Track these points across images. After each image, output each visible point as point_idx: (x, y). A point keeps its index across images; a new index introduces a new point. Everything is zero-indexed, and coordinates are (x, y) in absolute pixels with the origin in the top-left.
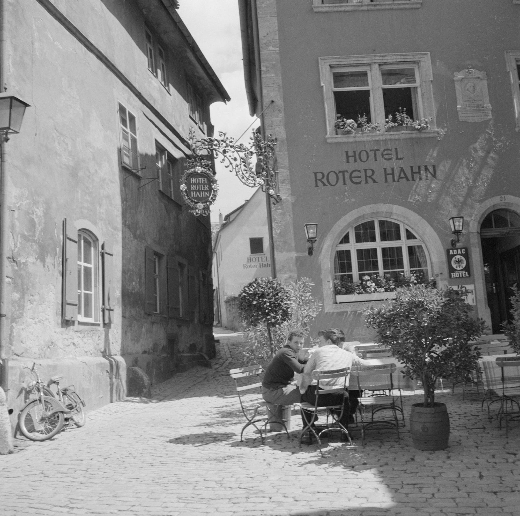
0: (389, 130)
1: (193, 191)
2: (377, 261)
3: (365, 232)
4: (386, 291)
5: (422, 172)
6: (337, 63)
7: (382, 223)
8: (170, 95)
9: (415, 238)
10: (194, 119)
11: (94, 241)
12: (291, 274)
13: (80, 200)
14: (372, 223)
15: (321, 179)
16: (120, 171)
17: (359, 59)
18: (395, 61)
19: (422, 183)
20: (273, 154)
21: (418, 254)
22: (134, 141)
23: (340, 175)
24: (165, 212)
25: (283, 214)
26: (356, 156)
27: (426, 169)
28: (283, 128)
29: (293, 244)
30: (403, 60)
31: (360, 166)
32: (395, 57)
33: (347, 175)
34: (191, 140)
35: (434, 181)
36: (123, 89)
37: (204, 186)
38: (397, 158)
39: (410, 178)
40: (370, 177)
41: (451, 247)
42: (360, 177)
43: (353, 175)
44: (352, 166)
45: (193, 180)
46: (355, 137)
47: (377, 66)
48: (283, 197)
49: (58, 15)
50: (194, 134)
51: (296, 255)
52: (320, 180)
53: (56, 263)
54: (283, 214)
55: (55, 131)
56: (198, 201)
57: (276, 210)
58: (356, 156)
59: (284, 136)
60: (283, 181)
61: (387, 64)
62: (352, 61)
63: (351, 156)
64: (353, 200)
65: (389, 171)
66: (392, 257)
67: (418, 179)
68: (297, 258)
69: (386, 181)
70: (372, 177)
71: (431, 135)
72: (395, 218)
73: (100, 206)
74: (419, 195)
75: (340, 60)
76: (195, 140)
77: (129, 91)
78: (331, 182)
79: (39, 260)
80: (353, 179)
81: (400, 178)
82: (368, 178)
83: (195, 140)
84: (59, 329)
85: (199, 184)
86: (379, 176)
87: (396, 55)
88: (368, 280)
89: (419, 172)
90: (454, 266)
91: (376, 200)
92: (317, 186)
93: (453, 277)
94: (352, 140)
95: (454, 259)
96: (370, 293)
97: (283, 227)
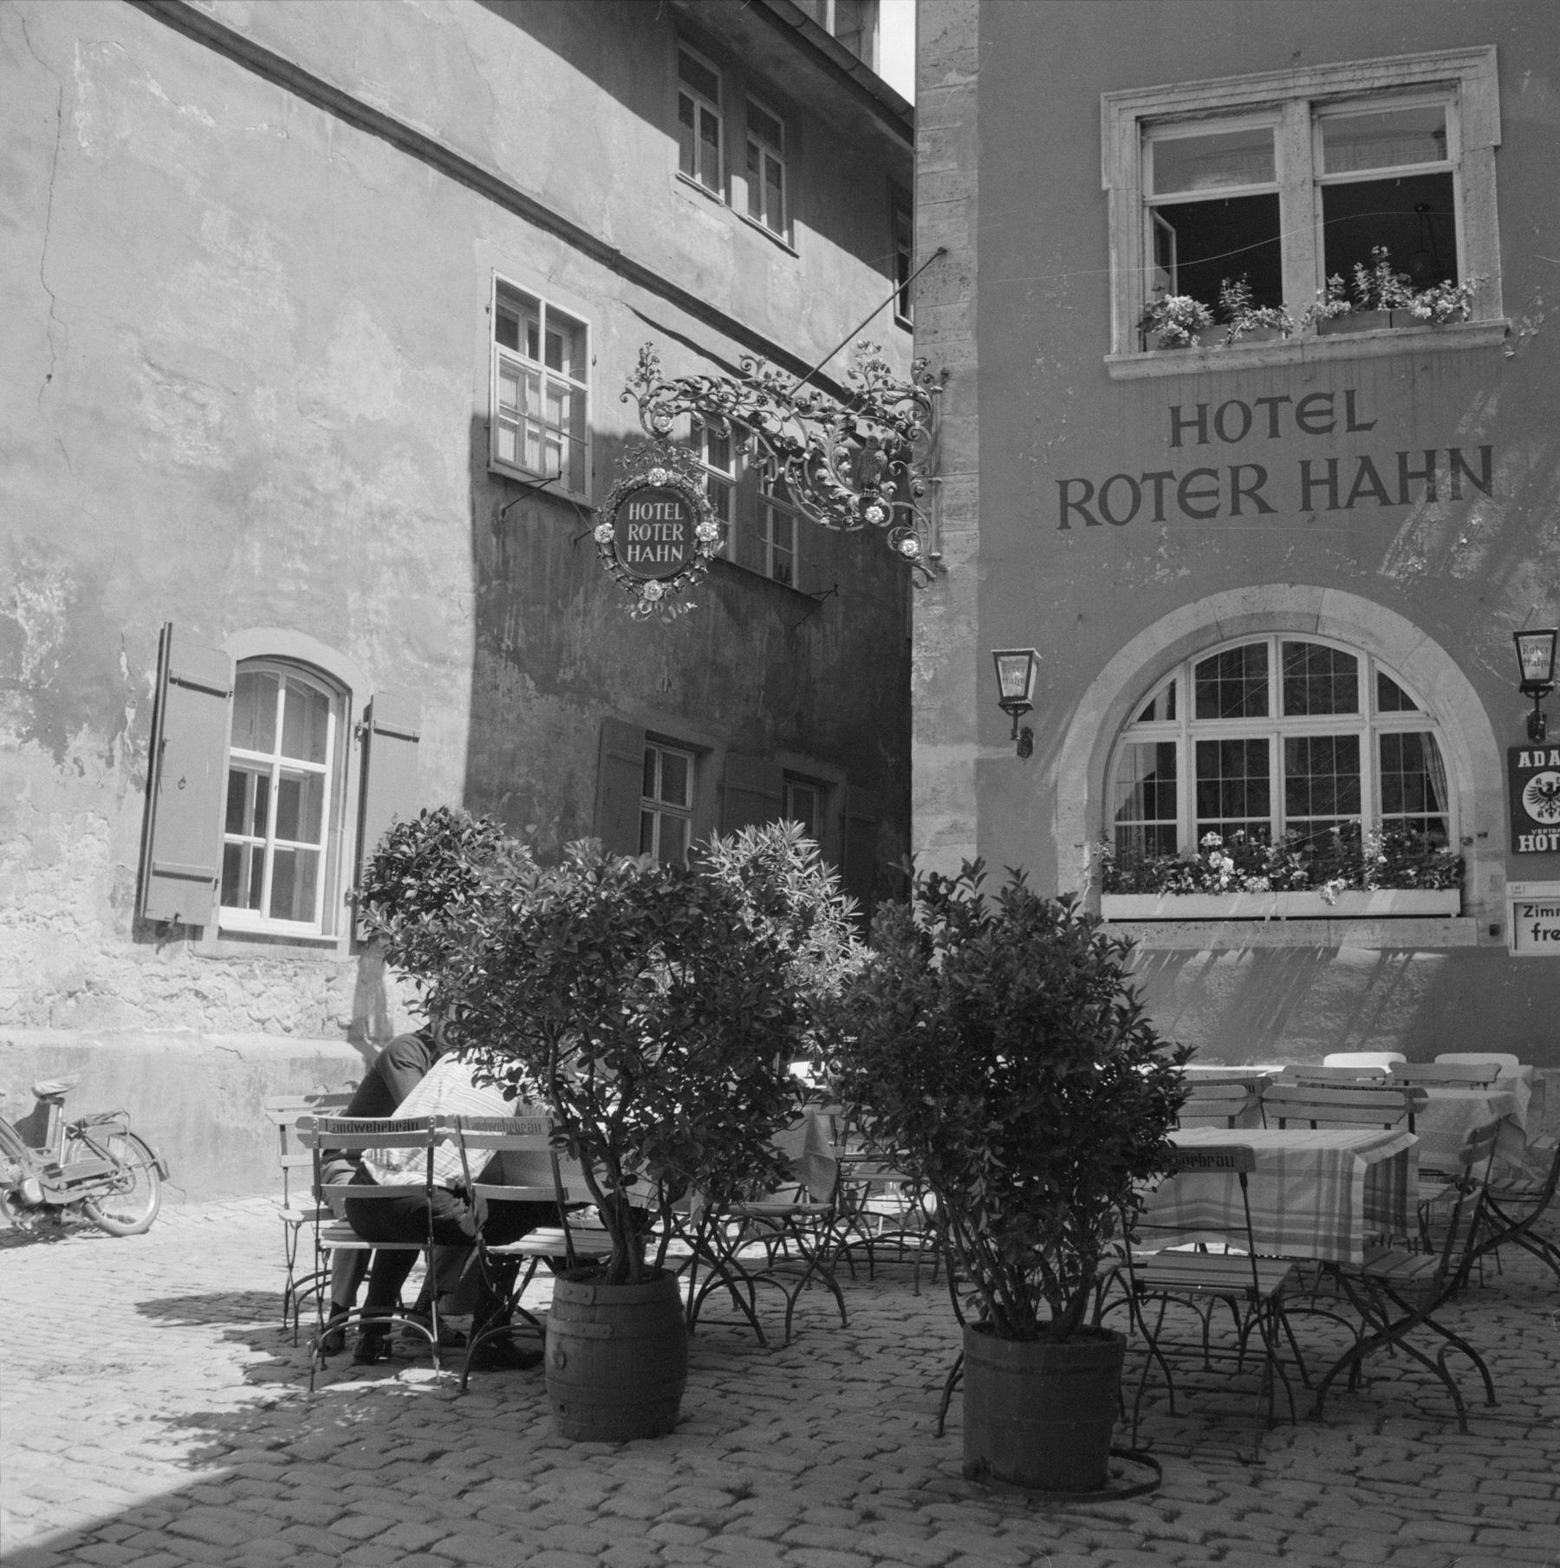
0: (1325, 325)
1: (634, 543)
2: (1266, 786)
3: (1228, 683)
4: (1276, 886)
5: (1439, 473)
6: (1163, 109)
7: (1293, 652)
8: (796, 256)
9: (1409, 705)
11: (338, 695)
12: (959, 817)
13: (257, 571)
14: (1258, 653)
15: (1081, 504)
16: (475, 485)
17: (1243, 88)
18: (1367, 84)
19: (1436, 513)
20: (928, 425)
21: (1430, 765)
22: (579, 398)
23: (1148, 488)
24: (722, 614)
25: (949, 619)
26: (1207, 423)
27: (1456, 461)
28: (969, 335)
29: (972, 719)
30: (1398, 81)
31: (1220, 455)
32: (1368, 73)
33: (1170, 488)
34: (644, 385)
35: (1483, 503)
36: (529, 237)
38: (1352, 427)
39: (1393, 493)
40: (1250, 493)
41: (1524, 738)
42: (1215, 493)
43: (1190, 488)
44: (1191, 454)
45: (636, 510)
46: (1202, 357)
47: (1302, 109)
48: (951, 563)
49: (206, 28)
50: (654, 367)
51: (976, 755)
52: (1078, 507)
53: (118, 753)
54: (949, 619)
55: (147, 368)
56: (646, 576)
57: (926, 605)
58: (1207, 423)
59: (972, 362)
61: (1344, 101)
62: (1214, 97)
63: (1189, 424)
64: (1184, 572)
65: (1320, 471)
66: (1323, 769)
67: (1423, 498)
68: (980, 763)
69: (1306, 506)
70: (1258, 492)
71: (1480, 340)
72: (1334, 633)
73: (366, 590)
74: (1420, 554)
75: (1173, 97)
76: (655, 384)
78: (1112, 509)
79: (35, 741)
80: (1190, 502)
81: (1356, 493)
82: (1242, 497)
83: (655, 384)
84: (127, 946)
85: (654, 520)
86: (1283, 489)
87: (1370, 66)
88: (1218, 848)
89: (1429, 474)
90: (1532, 809)
91: (1259, 573)
92: (1064, 524)
93: (1523, 849)
94: (1192, 366)
95: (1532, 783)
96: (1217, 893)
97: (945, 662)
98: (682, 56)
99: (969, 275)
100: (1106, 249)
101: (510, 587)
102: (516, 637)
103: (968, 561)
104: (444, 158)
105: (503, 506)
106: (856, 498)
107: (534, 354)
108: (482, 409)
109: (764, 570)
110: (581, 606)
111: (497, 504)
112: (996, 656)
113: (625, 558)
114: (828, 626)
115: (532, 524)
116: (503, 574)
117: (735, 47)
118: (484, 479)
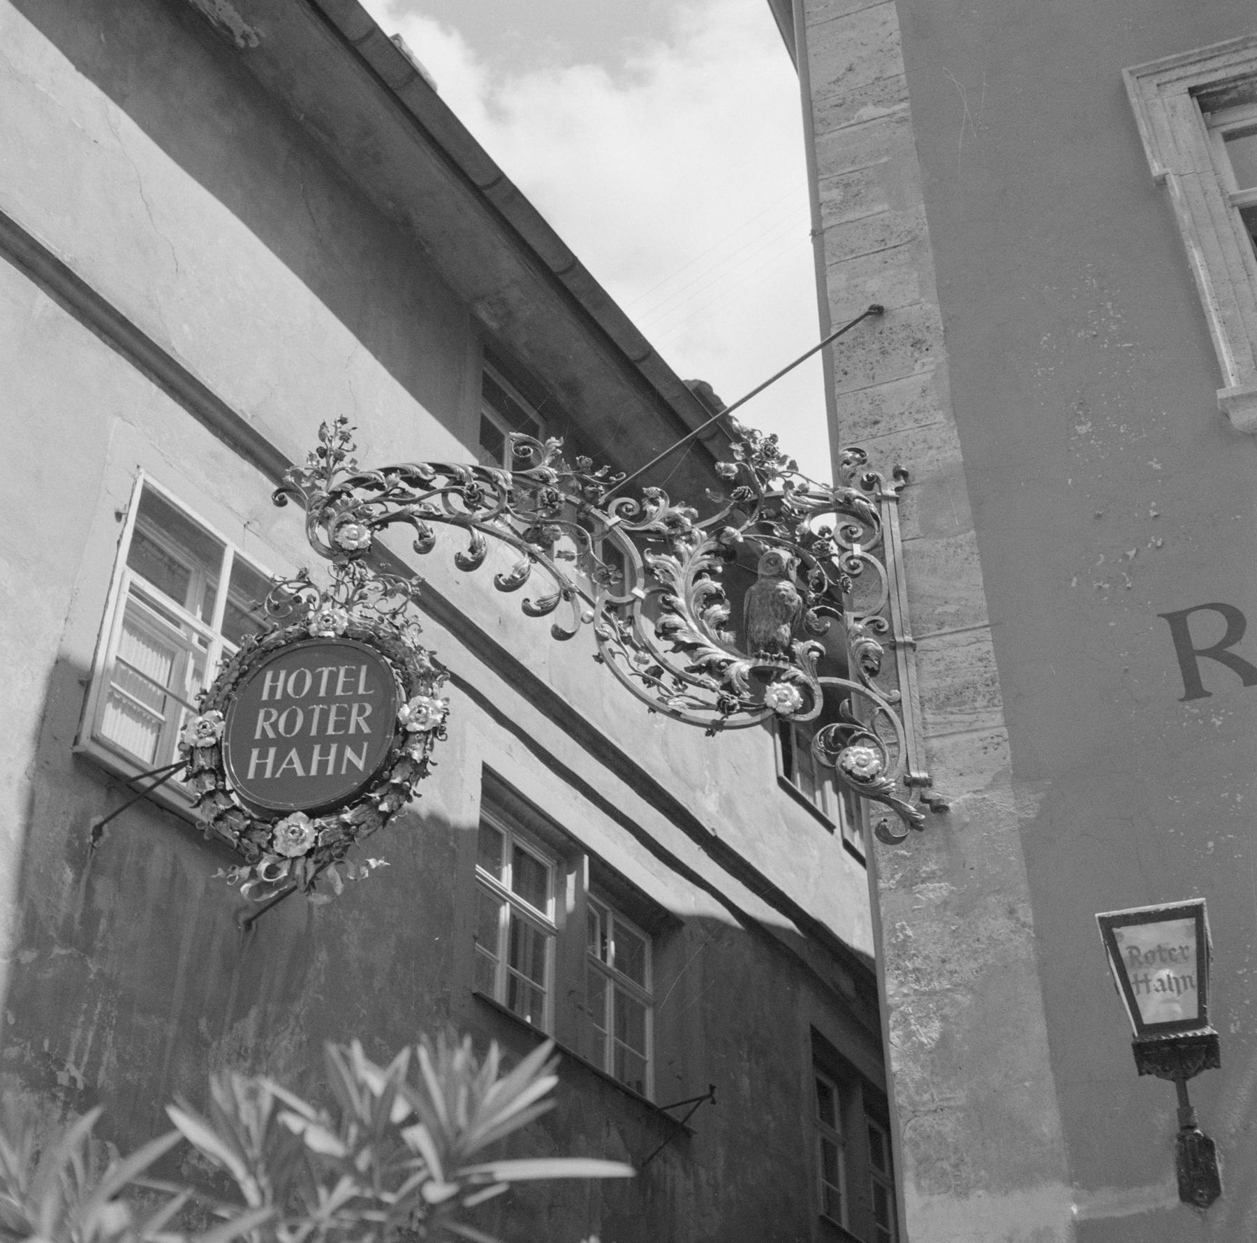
1: (264, 743)
10: (819, 808)
16: (42, 766)
28: (940, 417)
29: (1048, 1124)
37: (344, 713)
48: (954, 793)
57: (908, 884)
59: (953, 454)
60: (950, 700)
77: (25, 280)
85: (313, 695)
92: (1194, 689)
97: (964, 999)
98: (487, 380)
99: (930, 338)
100: (1181, 258)
101: (93, 966)
102: (94, 1066)
103: (990, 787)
104: (70, 288)
105: (97, 820)
106: (742, 666)
107: (207, 620)
108: (81, 653)
109: (601, 1060)
110: (251, 1042)
111: (85, 815)
112: (1108, 925)
113: (242, 767)
114: (702, 1171)
115: (157, 868)
116: (83, 935)
117: (562, 398)
118: (63, 762)
